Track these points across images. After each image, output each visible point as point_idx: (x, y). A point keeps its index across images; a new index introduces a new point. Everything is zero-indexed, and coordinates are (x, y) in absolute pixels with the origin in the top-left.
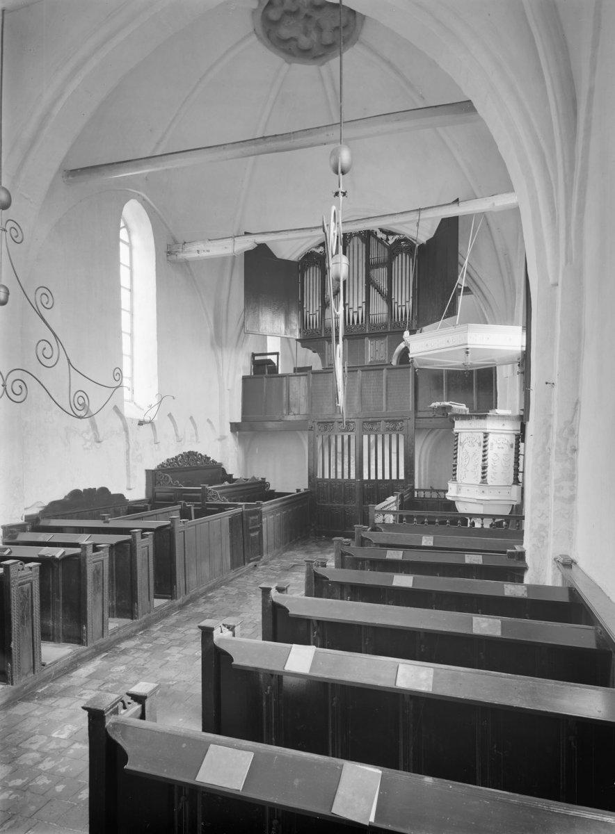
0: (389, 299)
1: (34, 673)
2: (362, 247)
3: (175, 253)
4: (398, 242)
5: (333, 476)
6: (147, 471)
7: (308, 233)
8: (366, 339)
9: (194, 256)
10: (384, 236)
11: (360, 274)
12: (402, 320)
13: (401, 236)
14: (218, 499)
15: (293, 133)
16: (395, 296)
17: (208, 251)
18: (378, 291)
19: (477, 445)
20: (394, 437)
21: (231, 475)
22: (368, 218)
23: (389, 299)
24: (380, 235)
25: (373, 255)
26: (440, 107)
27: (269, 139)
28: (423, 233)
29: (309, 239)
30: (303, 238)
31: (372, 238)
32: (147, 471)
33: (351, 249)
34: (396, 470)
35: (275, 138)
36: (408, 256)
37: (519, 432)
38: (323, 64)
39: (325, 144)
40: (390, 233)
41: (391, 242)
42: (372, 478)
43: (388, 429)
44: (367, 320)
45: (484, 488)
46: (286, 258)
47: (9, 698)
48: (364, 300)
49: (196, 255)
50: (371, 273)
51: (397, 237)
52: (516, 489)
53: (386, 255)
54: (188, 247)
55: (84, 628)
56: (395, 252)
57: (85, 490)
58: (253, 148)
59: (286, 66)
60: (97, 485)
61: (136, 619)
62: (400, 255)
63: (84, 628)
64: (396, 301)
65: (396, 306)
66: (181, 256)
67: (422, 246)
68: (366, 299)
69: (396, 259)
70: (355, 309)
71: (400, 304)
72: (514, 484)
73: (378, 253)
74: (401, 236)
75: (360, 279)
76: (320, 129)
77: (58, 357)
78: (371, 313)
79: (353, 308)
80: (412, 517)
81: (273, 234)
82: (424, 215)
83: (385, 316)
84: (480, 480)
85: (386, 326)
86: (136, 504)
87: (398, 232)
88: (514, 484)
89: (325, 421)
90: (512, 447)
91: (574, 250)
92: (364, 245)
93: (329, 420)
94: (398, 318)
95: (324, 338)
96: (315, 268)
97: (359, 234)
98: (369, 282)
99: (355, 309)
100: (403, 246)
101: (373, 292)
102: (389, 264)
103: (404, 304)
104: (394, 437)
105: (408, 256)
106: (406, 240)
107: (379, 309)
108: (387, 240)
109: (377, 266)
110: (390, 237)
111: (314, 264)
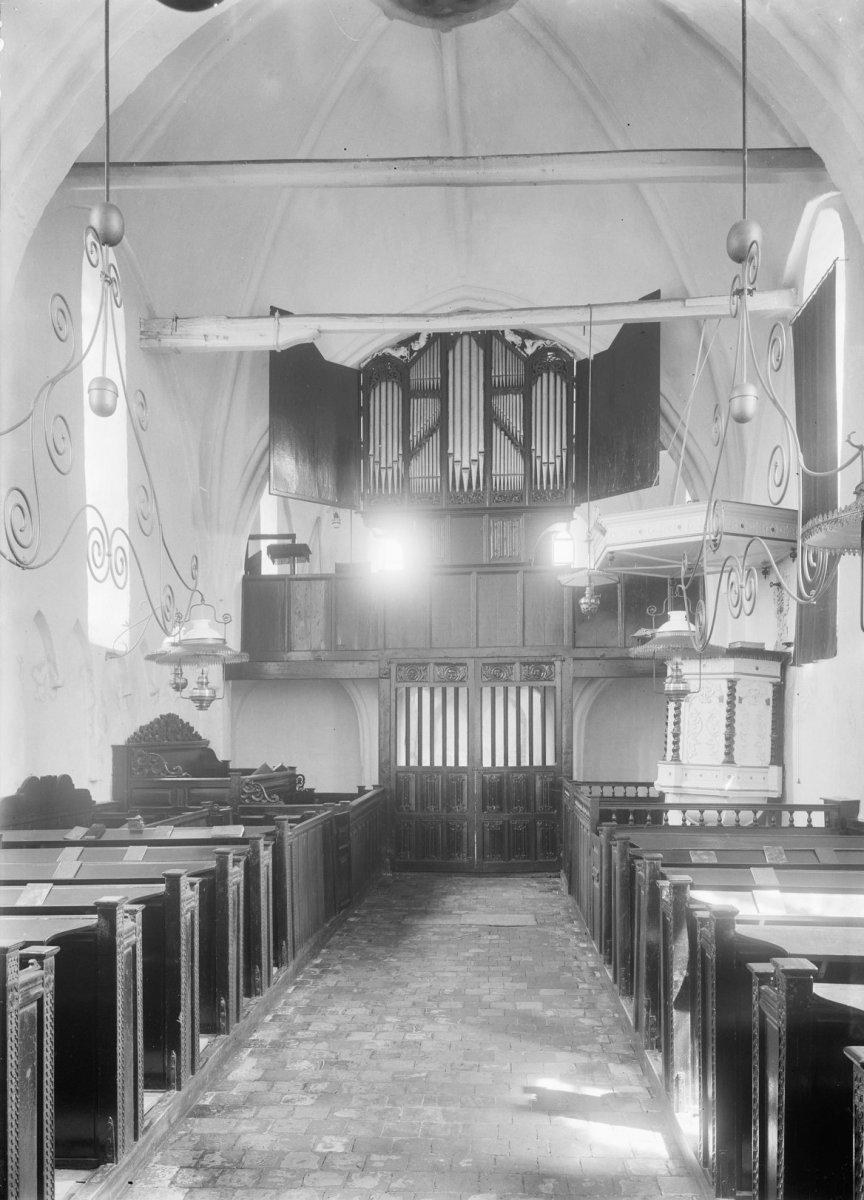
0: (525, 449)
1: (193, 1073)
2: (478, 355)
3: (157, 336)
4: (541, 352)
5: (426, 763)
6: (115, 748)
7: (363, 324)
8: (486, 517)
9: (200, 345)
10: (517, 340)
11: (474, 404)
12: (548, 488)
13: (548, 342)
14: (264, 798)
15: (484, 158)
16: (536, 445)
17: (226, 338)
18: (506, 434)
19: (715, 700)
20: (500, 691)
21: (226, 763)
22: (531, 309)
23: (525, 449)
24: (510, 337)
25: (498, 371)
26: (729, 153)
27: (439, 162)
28: (589, 342)
29: (376, 335)
30: (362, 332)
31: (495, 340)
32: (115, 748)
33: (458, 357)
34: (497, 753)
35: (450, 162)
36: (558, 378)
37: (779, 680)
38: (448, 30)
39: (535, 184)
40: (526, 335)
41: (530, 351)
42: (535, 764)
43: (528, 678)
44: (488, 484)
45: (728, 769)
46: (338, 360)
47: (181, 1110)
48: (482, 449)
49: (201, 343)
50: (494, 401)
51: (540, 343)
52: (775, 770)
53: (522, 372)
54: (184, 327)
55: (223, 1002)
56: (536, 368)
57: (43, 778)
58: (408, 173)
59: (384, 21)
60: (57, 773)
61: (257, 994)
62: (545, 375)
63: (223, 1002)
64: (539, 454)
65: (377, 467)
66: (168, 342)
67: (583, 364)
68: (485, 446)
69: (539, 381)
70: (466, 464)
71: (383, 465)
72: (772, 764)
73: (505, 370)
74: (548, 342)
75: (474, 412)
76: (531, 159)
77: (783, 496)
78: (494, 472)
79: (461, 462)
80: (627, 813)
81: (354, 319)
82: (598, 315)
83: (519, 479)
84: (723, 757)
85: (522, 498)
86: (106, 810)
87: (543, 335)
88: (772, 764)
89: (412, 661)
90: (768, 704)
91: (693, 393)
92: (481, 352)
93: (418, 661)
94: (542, 482)
95: (488, 509)
96: (390, 384)
97: (472, 334)
98: (491, 418)
99: (466, 464)
100: (547, 361)
101: (436, 439)
102: (525, 389)
103: (552, 460)
104: (500, 691)
105: (558, 378)
106: (556, 350)
107: (509, 466)
108: (523, 346)
109: (506, 390)
110: (528, 343)
111: (388, 376)
